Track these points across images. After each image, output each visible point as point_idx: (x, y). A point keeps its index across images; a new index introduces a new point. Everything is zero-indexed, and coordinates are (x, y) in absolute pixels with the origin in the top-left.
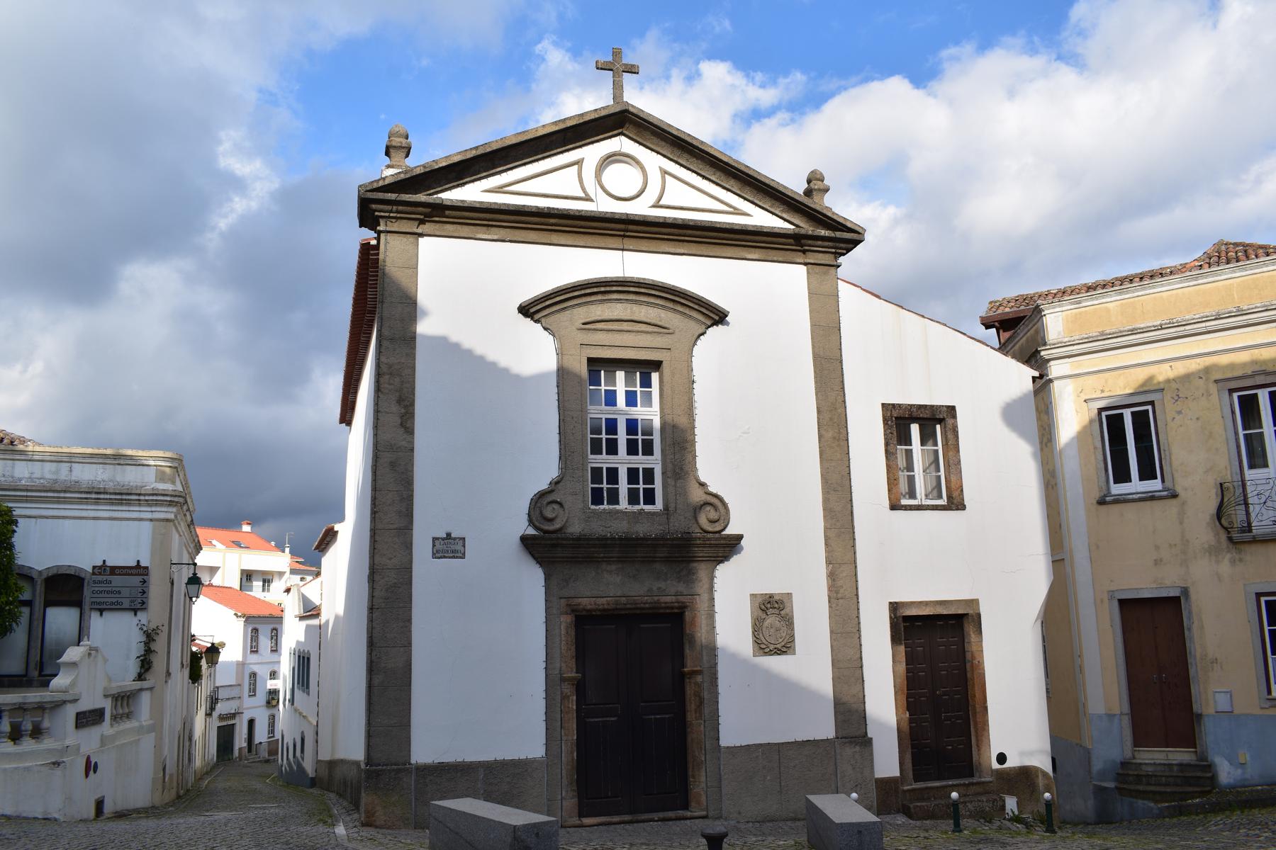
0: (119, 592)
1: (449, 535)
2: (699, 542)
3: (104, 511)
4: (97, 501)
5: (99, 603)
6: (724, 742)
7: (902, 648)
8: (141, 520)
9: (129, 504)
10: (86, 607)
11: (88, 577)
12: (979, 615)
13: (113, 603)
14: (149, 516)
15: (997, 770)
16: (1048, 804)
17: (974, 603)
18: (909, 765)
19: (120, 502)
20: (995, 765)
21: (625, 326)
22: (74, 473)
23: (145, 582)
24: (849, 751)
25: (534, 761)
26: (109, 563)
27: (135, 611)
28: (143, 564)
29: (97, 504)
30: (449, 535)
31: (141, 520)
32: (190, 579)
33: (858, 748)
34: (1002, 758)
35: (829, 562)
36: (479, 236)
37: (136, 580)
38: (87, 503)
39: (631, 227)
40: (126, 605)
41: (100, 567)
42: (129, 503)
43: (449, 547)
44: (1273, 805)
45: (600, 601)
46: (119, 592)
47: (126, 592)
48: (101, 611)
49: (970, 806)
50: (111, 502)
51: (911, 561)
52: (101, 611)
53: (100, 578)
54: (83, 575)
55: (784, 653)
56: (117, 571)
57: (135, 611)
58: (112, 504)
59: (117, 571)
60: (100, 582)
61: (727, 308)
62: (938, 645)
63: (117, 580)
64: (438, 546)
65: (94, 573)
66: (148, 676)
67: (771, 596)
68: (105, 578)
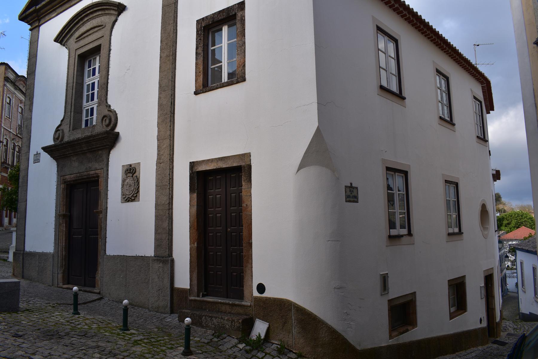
2: (110, 139)
6: (108, 253)
7: (195, 195)
12: (250, 167)
15: (256, 298)
16: (76, 295)
18: (195, 282)
20: (256, 294)
24: (157, 266)
25: (143, 258)
33: (161, 265)
34: (261, 288)
36: (72, 4)
45: (72, 176)
49: (215, 321)
51: (211, 128)
55: (133, 201)
61: (125, 4)
62: (222, 189)
67: (131, 165)
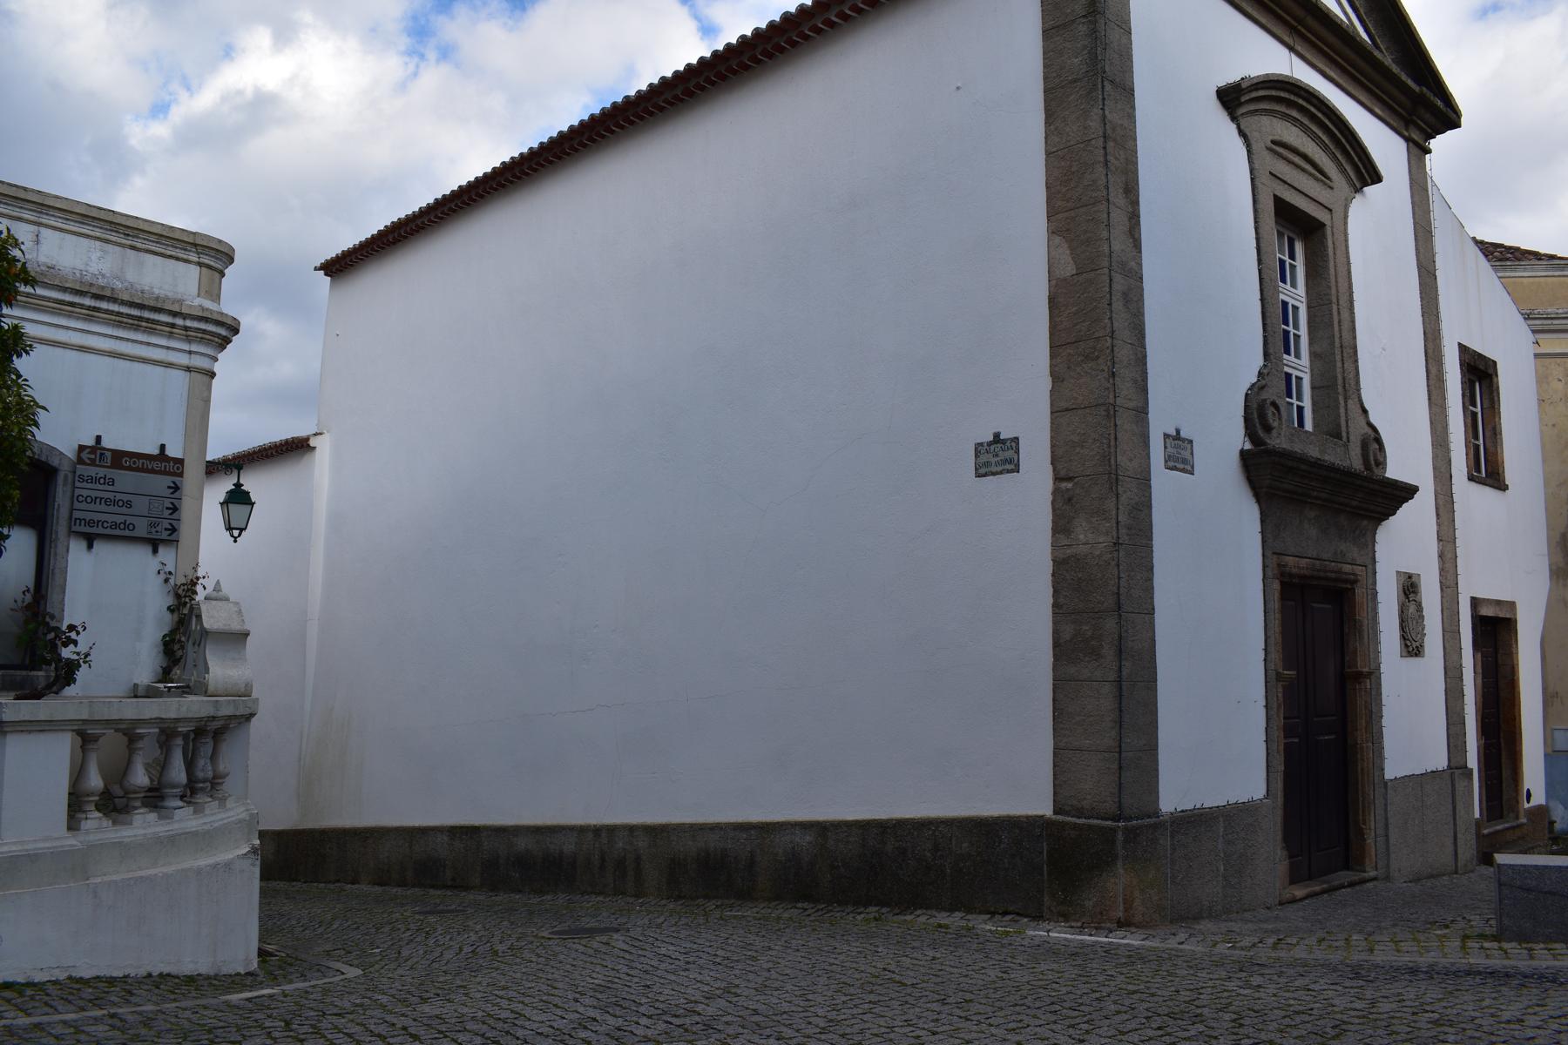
0: (129, 504)
1: (997, 435)
3: (100, 336)
4: (92, 314)
5: (89, 523)
6: (1037, 801)
8: (169, 365)
9: (151, 331)
10: (61, 528)
11: (65, 468)
13: (115, 525)
14: (183, 359)
17: (1512, 605)
19: (136, 324)
21: (1297, 160)
22: (44, 248)
23: (176, 488)
26: (107, 443)
27: (155, 545)
28: (170, 452)
29: (89, 319)
30: (997, 435)
31: (169, 365)
32: (230, 493)
35: (1440, 540)
37: (160, 483)
38: (70, 315)
39: (1310, 21)
40: (141, 531)
41: (93, 450)
42: (151, 327)
43: (997, 456)
44: (8, 986)
46: (129, 504)
47: (140, 505)
48: (90, 540)
50: (119, 321)
52: (90, 540)
53: (92, 471)
54: (55, 462)
56: (126, 462)
57: (155, 545)
58: (120, 325)
59: (126, 462)
60: (92, 480)
63: (126, 480)
64: (984, 458)
65: (80, 461)
66: (177, 671)
68: (102, 472)
